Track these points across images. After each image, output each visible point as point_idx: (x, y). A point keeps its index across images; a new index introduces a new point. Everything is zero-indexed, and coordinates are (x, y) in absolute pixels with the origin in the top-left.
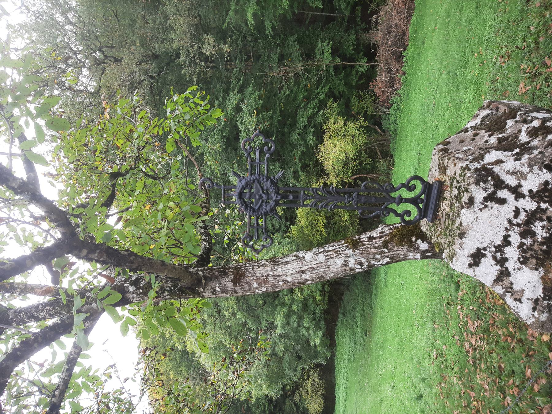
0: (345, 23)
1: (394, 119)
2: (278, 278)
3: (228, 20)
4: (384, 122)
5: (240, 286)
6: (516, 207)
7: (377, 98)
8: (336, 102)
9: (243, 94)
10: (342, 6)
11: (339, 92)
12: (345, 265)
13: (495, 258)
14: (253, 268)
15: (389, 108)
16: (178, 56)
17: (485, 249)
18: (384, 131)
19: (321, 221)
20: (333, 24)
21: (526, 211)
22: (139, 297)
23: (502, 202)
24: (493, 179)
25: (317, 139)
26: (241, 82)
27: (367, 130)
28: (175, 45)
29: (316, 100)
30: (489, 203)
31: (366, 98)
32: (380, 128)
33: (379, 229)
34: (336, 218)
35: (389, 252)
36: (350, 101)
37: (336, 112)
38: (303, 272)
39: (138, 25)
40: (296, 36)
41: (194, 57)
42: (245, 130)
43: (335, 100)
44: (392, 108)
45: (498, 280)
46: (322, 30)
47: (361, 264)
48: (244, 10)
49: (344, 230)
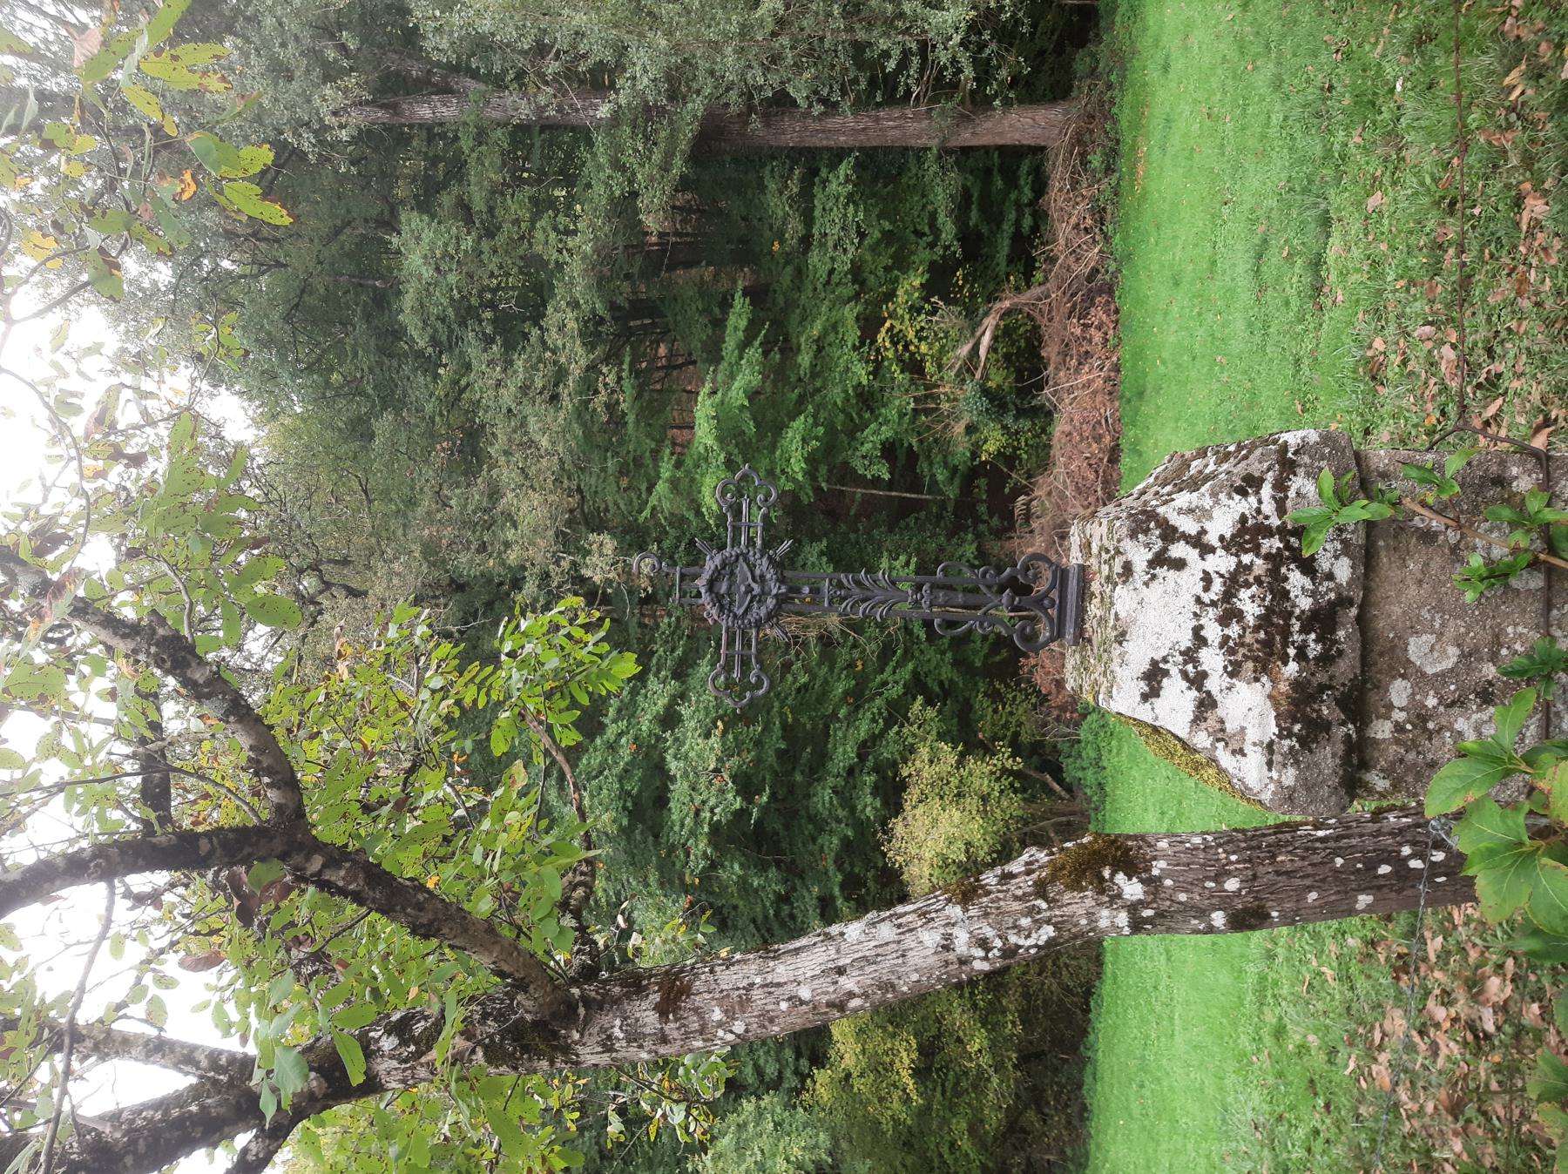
0: (949, 515)
1: (1093, 755)
2: (778, 991)
3: (653, 501)
4: (1068, 764)
5: (676, 1020)
6: (1204, 572)
7: (1044, 699)
8: (933, 706)
9: (683, 683)
10: (940, 477)
11: (941, 684)
12: (946, 948)
13: (1185, 674)
14: (712, 971)
15: (1077, 725)
16: (517, 584)
17: (1165, 660)
18: (1069, 789)
19: (905, 1058)
20: (917, 519)
21: (1222, 576)
22: (405, 1070)
23: (1179, 564)
24: (1158, 525)
25: (885, 803)
26: (679, 652)
27: (1021, 783)
28: (512, 557)
29: (878, 701)
30: (1158, 571)
31: (1015, 698)
32: (1060, 782)
33: (1025, 857)
34: (951, 1049)
35: (1050, 908)
36: (971, 707)
37: (934, 732)
38: (841, 971)
39: (420, 511)
40: (825, 543)
41: (559, 586)
42: (685, 775)
43: (929, 702)
44: (1085, 726)
45: (1198, 719)
46: (891, 530)
47: (984, 944)
48: (693, 480)
49: (975, 1087)
